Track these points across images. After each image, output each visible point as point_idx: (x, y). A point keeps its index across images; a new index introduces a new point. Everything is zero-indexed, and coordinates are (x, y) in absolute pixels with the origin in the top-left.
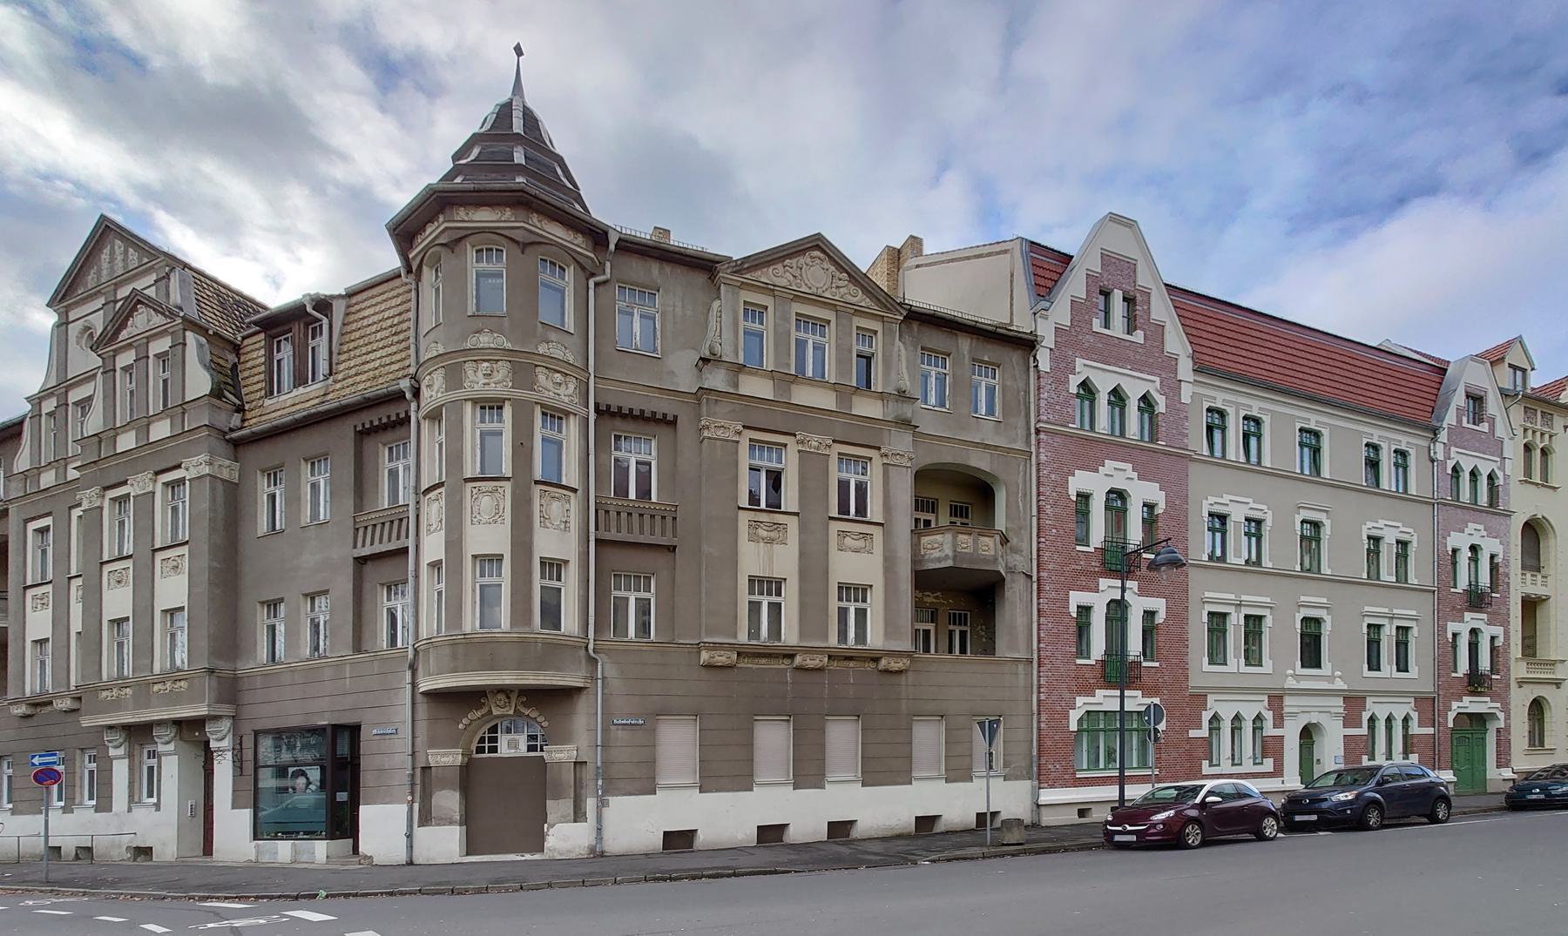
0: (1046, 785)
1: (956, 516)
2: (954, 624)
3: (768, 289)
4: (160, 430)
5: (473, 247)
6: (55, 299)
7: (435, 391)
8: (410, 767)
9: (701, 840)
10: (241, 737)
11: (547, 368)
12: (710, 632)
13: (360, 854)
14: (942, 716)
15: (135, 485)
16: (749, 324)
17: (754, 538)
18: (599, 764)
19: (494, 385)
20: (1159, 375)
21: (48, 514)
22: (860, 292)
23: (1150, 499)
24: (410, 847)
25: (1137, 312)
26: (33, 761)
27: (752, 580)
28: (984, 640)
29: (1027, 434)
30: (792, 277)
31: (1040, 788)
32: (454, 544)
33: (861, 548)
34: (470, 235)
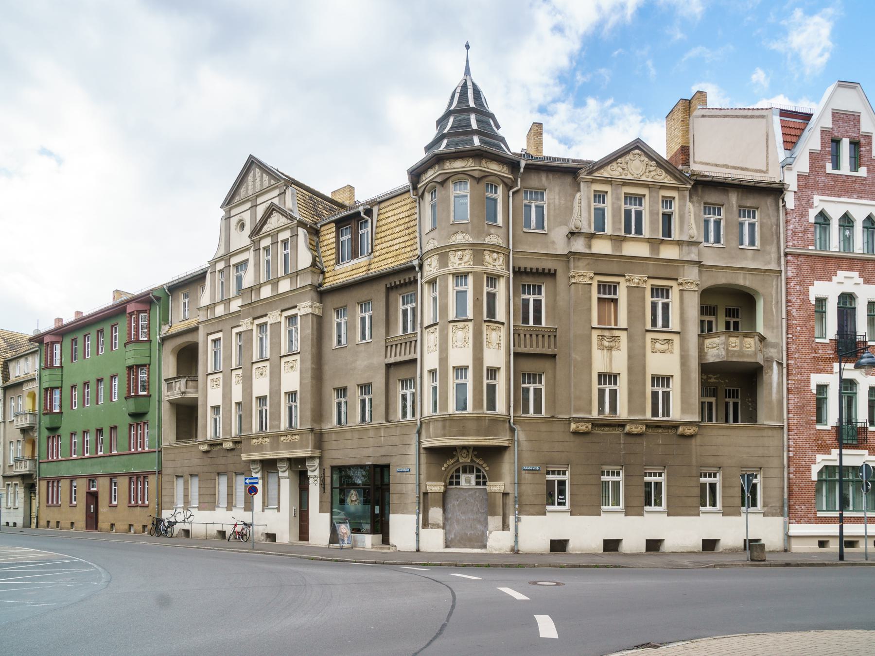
0: (794, 521)
1: (730, 316)
3: (608, 181)
4: (285, 286)
6: (225, 203)
7: (432, 268)
9: (571, 545)
10: (324, 470)
12: (577, 410)
14: (720, 468)
15: (271, 317)
17: (601, 347)
18: (516, 495)
21: (221, 331)
22: (664, 172)
24: (418, 541)
25: (861, 153)
26: (246, 481)
27: (600, 375)
28: (751, 409)
31: (790, 523)
32: (443, 360)
34: (452, 176)
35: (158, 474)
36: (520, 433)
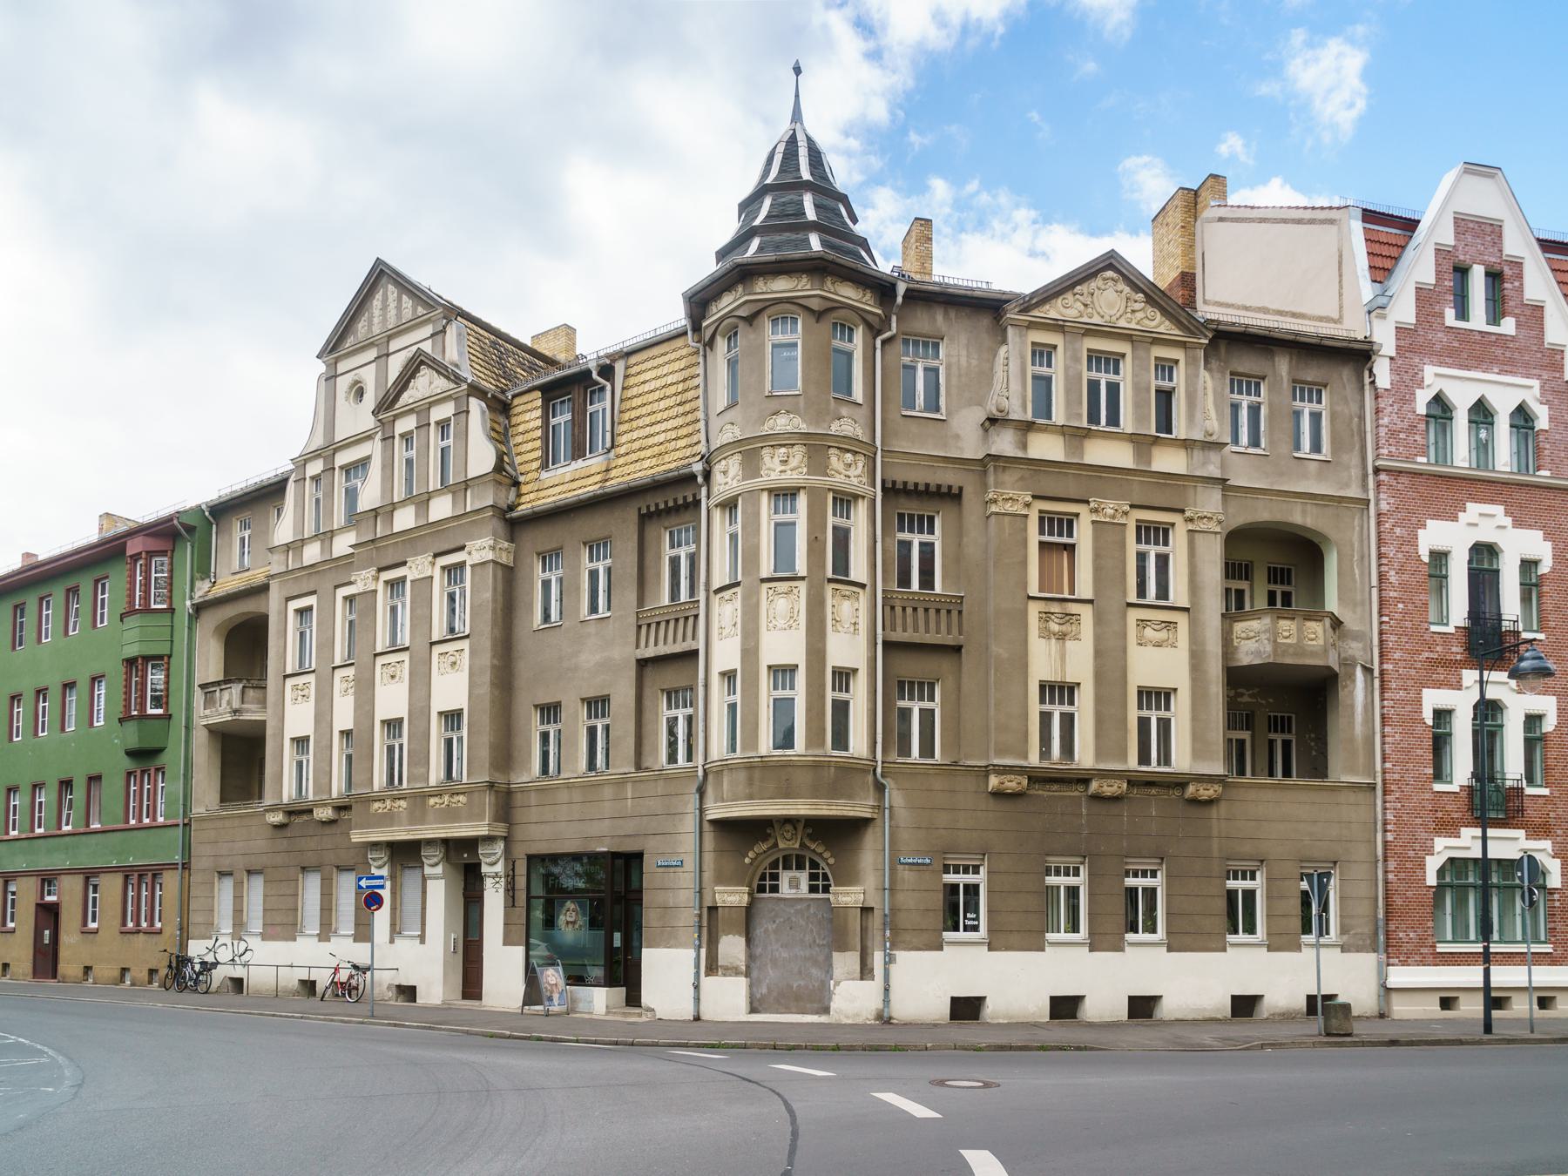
0: (1396, 961)
1: (1275, 582)
2: (1276, 731)
3: (1058, 326)
4: (441, 508)
5: (769, 317)
7: (728, 478)
8: (697, 907)
10: (514, 862)
11: (839, 448)
12: (1001, 752)
13: (643, 1005)
14: (1262, 861)
16: (1037, 368)
17: (1046, 634)
18: (887, 912)
19: (789, 472)
20: (1539, 377)
22: (1158, 314)
23: (1531, 554)
24: (697, 1000)
27: (1042, 687)
28: (1314, 753)
29: (1363, 474)
30: (1082, 307)
31: (1388, 965)
32: (750, 652)
33: (1163, 642)
34: (770, 305)
35: (183, 868)
36: (895, 793)
